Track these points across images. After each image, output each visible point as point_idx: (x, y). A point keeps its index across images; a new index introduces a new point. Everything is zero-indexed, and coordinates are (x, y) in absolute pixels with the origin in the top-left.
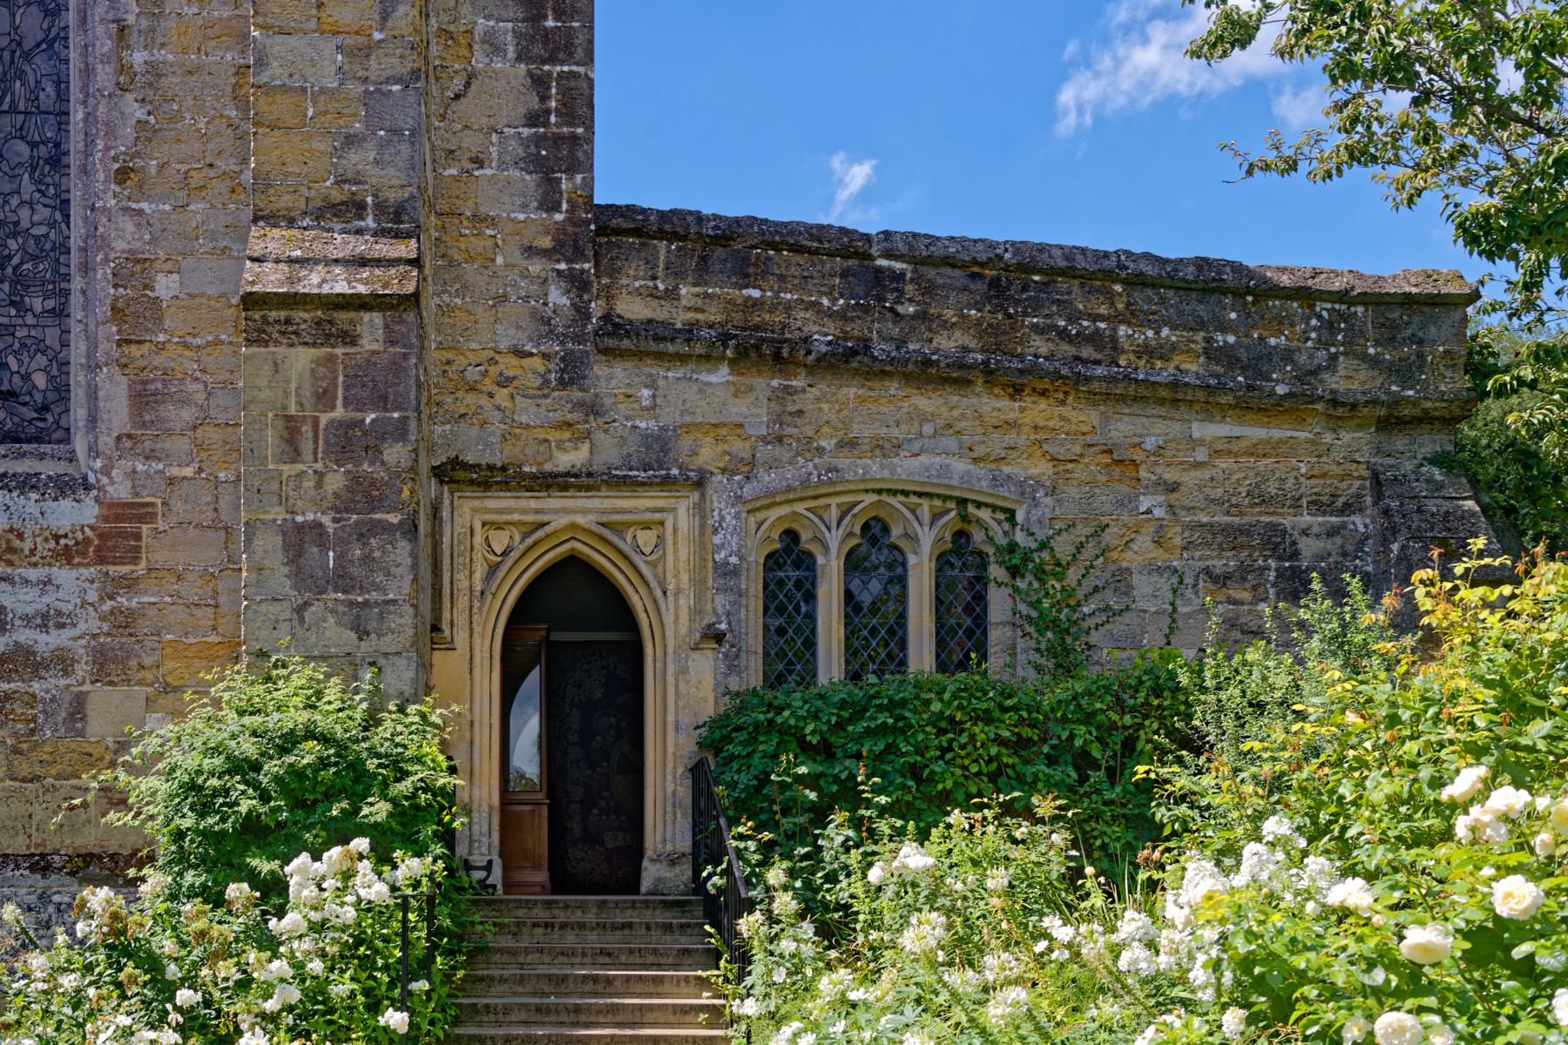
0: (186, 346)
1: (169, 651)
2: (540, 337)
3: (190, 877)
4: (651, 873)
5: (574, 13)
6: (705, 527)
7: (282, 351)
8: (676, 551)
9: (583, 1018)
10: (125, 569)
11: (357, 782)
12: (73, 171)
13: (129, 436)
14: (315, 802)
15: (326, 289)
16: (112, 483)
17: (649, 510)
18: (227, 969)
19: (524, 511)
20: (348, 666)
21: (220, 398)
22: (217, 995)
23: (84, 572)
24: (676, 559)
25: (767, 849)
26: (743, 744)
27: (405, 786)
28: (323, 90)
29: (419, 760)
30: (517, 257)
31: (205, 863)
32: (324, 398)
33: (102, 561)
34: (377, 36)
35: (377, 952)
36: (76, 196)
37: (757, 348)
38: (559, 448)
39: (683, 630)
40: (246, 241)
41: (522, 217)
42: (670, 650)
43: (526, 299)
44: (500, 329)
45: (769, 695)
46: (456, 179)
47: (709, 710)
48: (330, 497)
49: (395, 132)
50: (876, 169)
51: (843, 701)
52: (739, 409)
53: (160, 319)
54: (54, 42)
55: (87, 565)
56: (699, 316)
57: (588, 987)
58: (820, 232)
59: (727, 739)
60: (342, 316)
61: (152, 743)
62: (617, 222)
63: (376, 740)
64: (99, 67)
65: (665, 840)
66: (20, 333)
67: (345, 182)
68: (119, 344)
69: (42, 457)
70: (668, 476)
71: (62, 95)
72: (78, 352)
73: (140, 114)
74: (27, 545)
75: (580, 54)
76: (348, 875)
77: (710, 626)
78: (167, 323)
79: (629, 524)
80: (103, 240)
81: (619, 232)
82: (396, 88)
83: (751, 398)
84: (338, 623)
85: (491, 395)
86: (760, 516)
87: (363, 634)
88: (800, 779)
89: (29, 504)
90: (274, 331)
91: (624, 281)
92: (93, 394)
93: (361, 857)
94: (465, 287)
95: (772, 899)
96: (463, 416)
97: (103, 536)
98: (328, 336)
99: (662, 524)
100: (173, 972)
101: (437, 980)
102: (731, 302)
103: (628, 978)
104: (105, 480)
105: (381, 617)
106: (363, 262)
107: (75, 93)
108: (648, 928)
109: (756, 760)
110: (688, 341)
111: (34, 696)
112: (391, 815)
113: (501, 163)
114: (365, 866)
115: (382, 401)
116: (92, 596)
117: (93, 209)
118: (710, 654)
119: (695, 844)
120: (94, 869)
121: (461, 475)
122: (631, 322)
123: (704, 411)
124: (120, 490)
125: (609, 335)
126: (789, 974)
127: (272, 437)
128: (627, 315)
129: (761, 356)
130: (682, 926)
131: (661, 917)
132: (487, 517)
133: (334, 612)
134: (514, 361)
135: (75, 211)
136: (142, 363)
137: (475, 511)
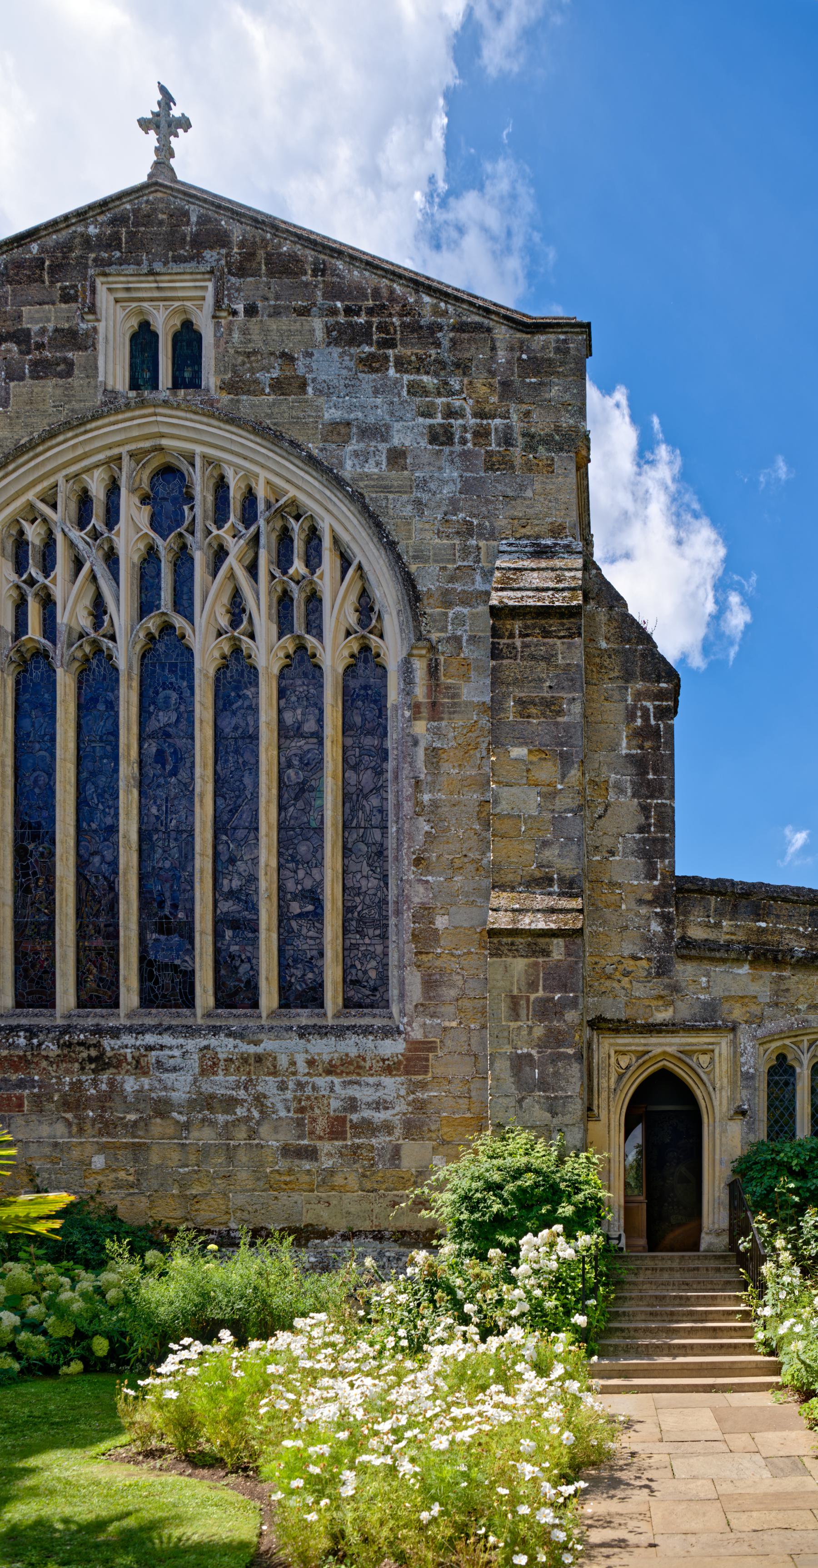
0: (452, 955)
1: (444, 1122)
2: (646, 949)
3: (465, 1245)
4: (706, 1240)
5: (664, 771)
6: (736, 1054)
7: (509, 960)
8: (720, 1066)
9: (675, 1318)
10: (420, 1077)
11: (554, 1195)
12: (390, 859)
13: (422, 1005)
14: (533, 1205)
15: (533, 926)
16: (413, 1030)
17: (706, 1044)
18: (492, 1294)
19: (637, 1045)
20: (546, 1132)
21: (471, 984)
22: (485, 1307)
23: (399, 1079)
24: (721, 1070)
25: (772, 1228)
26: (759, 1171)
27: (580, 1197)
28: (530, 817)
29: (587, 1183)
30: (633, 905)
31: (473, 1238)
32: (533, 986)
33: (407, 1073)
34: (559, 787)
35: (568, 1284)
36: (392, 873)
37: (764, 954)
38: (657, 1010)
39: (724, 1109)
40: (488, 899)
41: (636, 883)
42: (717, 1120)
43: (638, 928)
44: (624, 945)
45: (772, 1145)
46: (599, 862)
47: (738, 1153)
48: (536, 1040)
49: (569, 839)
50: (809, 835)
51: (812, 1148)
52: (754, 988)
53: (438, 940)
54: (379, 789)
55: (400, 1075)
56: (733, 937)
57: (677, 1302)
58: (798, 891)
59: (750, 1168)
60: (542, 941)
61: (441, 1174)
62: (688, 886)
63: (564, 1172)
64: (405, 803)
65: (714, 1223)
66: (363, 948)
67: (543, 866)
68: (416, 954)
69: (374, 1016)
70: (716, 1025)
71: (384, 820)
72: (393, 958)
73: (427, 828)
74: (368, 1064)
75: (667, 793)
76: (552, 1245)
77: (739, 1107)
78: (442, 943)
79: (695, 1052)
80: (407, 896)
81: (689, 891)
82: (570, 815)
83: (761, 982)
84: (541, 1108)
85: (619, 981)
86: (766, 1046)
87: (554, 1114)
88: (790, 1190)
89: (368, 1042)
90: (505, 949)
91: (692, 918)
92: (402, 982)
93: (558, 1235)
94: (605, 922)
95: (778, 1255)
96: (604, 992)
97: (408, 1059)
98: (534, 952)
99: (713, 1051)
100: (460, 1294)
101: (601, 1299)
102: (750, 929)
103: (698, 1297)
104: (409, 1029)
105: (564, 1105)
106: (552, 911)
107: (391, 817)
108: (707, 1269)
109: (765, 1180)
110: (727, 951)
111: (373, 1146)
112: (574, 1213)
113: (624, 853)
114: (561, 1240)
115: (564, 988)
116: (403, 1092)
117: (401, 880)
118: (739, 1122)
119: (731, 1225)
120: (407, 1239)
121: (603, 1025)
122: (696, 941)
123: (736, 990)
124: (417, 1034)
125: (684, 948)
126: (788, 1293)
127: (504, 1007)
128: (694, 937)
129: (766, 959)
130: (725, 1269)
131: (713, 1264)
132: (617, 1048)
133: (538, 1102)
134: (632, 962)
135: (391, 882)
136: (429, 965)
137: (611, 1045)
